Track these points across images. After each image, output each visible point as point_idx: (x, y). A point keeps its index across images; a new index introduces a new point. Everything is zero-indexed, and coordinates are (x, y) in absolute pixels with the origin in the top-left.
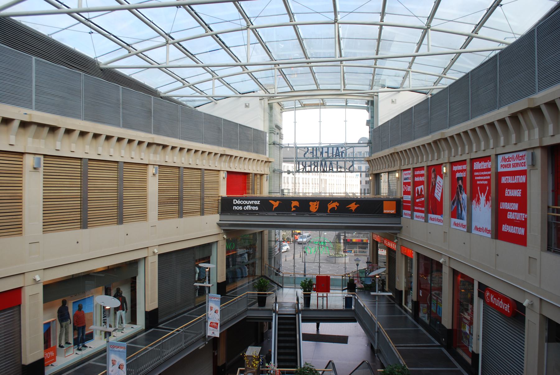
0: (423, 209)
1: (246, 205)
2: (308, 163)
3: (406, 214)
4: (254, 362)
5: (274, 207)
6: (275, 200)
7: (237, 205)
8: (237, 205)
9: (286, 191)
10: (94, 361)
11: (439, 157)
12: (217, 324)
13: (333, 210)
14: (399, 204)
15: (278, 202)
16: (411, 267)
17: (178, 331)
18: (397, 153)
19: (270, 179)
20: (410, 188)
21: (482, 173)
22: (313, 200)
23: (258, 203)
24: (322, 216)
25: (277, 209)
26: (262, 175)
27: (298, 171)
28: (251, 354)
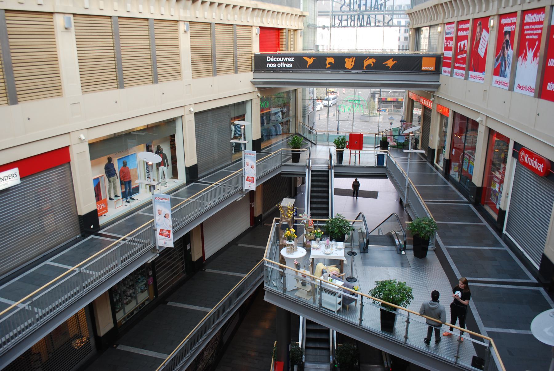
0: (464, 66)
1: (280, 62)
2: (345, 17)
3: (445, 72)
4: (288, 212)
5: (309, 64)
6: (310, 56)
7: (270, 62)
8: (270, 62)
9: (320, 48)
11: (487, 9)
12: (169, 232)
13: (369, 67)
14: (439, 61)
15: (312, 59)
17: (124, 240)
18: (442, 4)
19: (304, 35)
20: (452, 44)
22: (349, 56)
23: (292, 59)
24: (357, 73)
25: (311, 66)
26: (295, 30)
27: (334, 26)
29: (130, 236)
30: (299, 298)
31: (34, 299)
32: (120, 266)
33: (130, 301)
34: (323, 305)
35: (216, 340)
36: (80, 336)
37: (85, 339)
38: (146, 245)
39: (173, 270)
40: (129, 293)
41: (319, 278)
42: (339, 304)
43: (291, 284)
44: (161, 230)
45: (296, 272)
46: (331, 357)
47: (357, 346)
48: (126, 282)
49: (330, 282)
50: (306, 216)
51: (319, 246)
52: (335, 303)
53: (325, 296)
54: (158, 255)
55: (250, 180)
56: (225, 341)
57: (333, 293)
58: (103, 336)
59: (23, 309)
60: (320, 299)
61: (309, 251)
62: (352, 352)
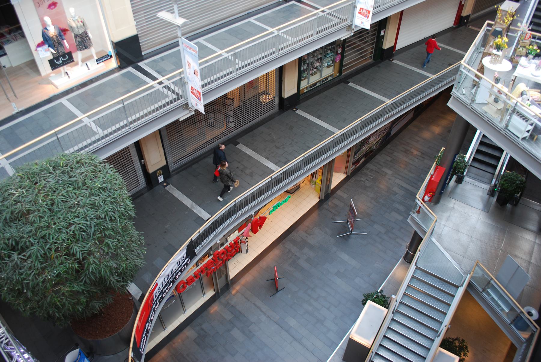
4: (506, 18)
10: (255, 19)
12: (369, 12)
16: (490, 295)
17: (323, 11)
21: (260, 62)
28: (506, 9)
29: (329, 9)
30: (486, 113)
31: (237, 51)
32: (315, 37)
33: (315, 73)
34: (509, 128)
35: (384, 130)
36: (267, 93)
37: (270, 97)
38: (343, 21)
39: (361, 53)
40: (316, 65)
41: (515, 99)
42: (528, 131)
43: (483, 96)
44: (361, 9)
45: (493, 86)
46: (494, 180)
47: (526, 178)
48: (316, 55)
49: (527, 106)
50: (524, 26)
51: (528, 65)
52: (523, 129)
53: (515, 118)
54: (352, 34)
55: (364, 13)
56: (393, 132)
57: (526, 118)
58: (287, 98)
59: (227, 59)
60: (509, 121)
61: (514, 68)
62: (518, 182)
